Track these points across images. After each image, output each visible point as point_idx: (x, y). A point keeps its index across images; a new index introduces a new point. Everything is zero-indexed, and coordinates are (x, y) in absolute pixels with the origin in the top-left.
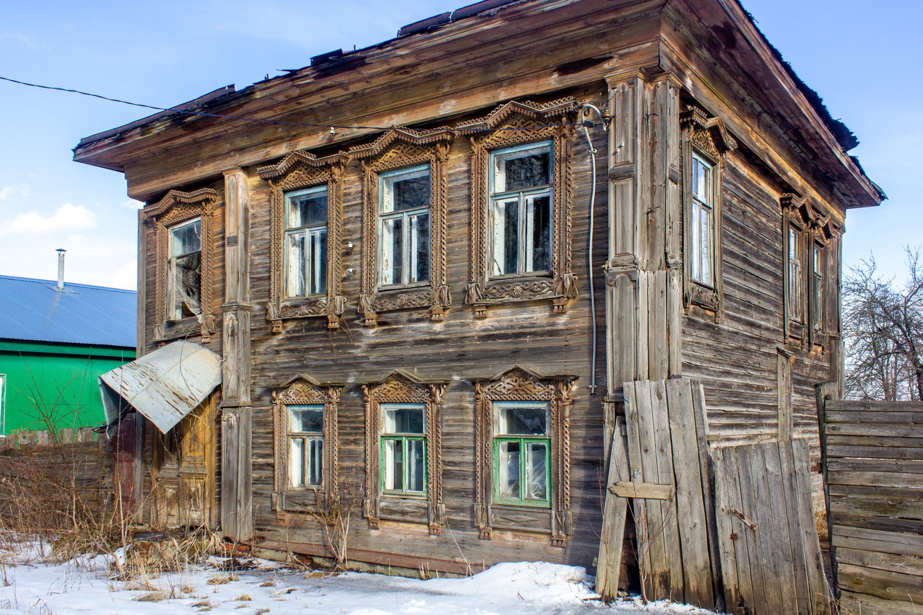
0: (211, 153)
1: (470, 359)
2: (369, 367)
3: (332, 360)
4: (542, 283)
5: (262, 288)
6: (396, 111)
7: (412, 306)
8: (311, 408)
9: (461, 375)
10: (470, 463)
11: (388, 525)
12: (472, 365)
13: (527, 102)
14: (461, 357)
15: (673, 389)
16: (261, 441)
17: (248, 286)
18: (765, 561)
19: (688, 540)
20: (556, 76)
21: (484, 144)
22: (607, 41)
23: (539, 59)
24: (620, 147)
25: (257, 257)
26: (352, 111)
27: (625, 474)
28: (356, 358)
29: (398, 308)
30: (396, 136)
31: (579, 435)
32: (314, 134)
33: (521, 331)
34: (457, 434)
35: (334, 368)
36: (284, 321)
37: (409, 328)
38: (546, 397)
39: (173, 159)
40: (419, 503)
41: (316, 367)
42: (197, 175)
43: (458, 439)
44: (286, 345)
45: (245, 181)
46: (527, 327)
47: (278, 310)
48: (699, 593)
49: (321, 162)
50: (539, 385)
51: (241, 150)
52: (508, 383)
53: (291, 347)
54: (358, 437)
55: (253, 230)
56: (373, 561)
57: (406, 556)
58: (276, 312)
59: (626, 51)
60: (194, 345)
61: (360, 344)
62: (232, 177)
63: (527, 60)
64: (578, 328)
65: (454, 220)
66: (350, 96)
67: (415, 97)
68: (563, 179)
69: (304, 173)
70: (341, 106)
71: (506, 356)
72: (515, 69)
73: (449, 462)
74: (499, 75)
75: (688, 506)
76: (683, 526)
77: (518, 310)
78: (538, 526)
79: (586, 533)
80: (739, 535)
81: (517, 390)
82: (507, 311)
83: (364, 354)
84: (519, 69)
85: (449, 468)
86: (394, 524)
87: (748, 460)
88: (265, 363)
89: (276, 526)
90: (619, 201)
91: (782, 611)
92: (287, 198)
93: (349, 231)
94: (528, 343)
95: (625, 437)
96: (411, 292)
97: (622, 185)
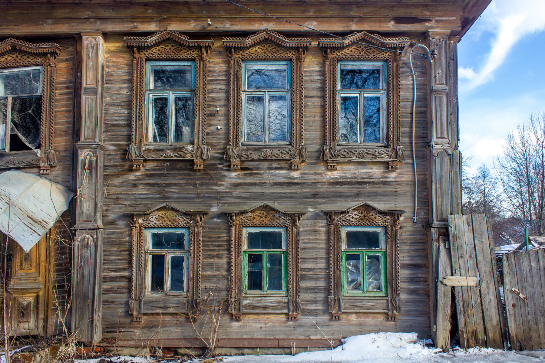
0: (68, 16)
1: (322, 198)
2: (233, 200)
3: (195, 194)
4: (381, 151)
6: (267, 19)
7: (275, 158)
8: (172, 231)
9: (315, 208)
10: (323, 269)
11: (249, 318)
12: (324, 202)
13: (375, 35)
14: (315, 195)
15: (476, 220)
16: (113, 257)
17: (103, 130)
18: (530, 318)
19: (487, 310)
20: (392, 23)
21: (240, 56)
22: (428, 10)
23: (382, 10)
24: (439, 74)
25: (112, 108)
26: (226, 11)
27: (449, 272)
28: (219, 193)
29: (262, 158)
30: (266, 37)
31: (406, 249)
32: (186, 21)
33: (362, 180)
34: (311, 249)
35: (197, 200)
36: (145, 161)
37: (269, 174)
38: (384, 224)
39: (17, 11)
40: (280, 299)
41: (178, 198)
42: (46, 31)
43: (311, 253)
44: (145, 180)
45: (103, 45)
46: (367, 178)
47: (140, 151)
48: (494, 340)
49: (193, 43)
50: (379, 216)
51: (103, 19)
52: (356, 215)
53: (151, 181)
54: (221, 253)
55: (108, 85)
56: (241, 345)
57: (266, 339)
58: (137, 153)
59: (440, 18)
60: (31, 175)
61: (223, 183)
62: (90, 39)
63: (374, 9)
64: (404, 181)
65: (308, 102)
67: (284, 13)
68: (395, 87)
69: (170, 49)
70: (215, 5)
71: (351, 196)
72: (364, 12)
73: (305, 269)
74: (353, 13)
75: (486, 289)
76: (485, 301)
77: (360, 167)
78: (378, 309)
79: (411, 311)
80: (516, 304)
81: (362, 219)
82: (352, 167)
83: (227, 191)
84: (368, 13)
85: (304, 273)
86: (255, 317)
87: (521, 261)
88: (121, 194)
89: (130, 328)
90: (438, 106)
91: (540, 345)
92: (148, 66)
93: (213, 98)
94: (368, 189)
95: (449, 250)
96: (274, 148)
97: (440, 97)
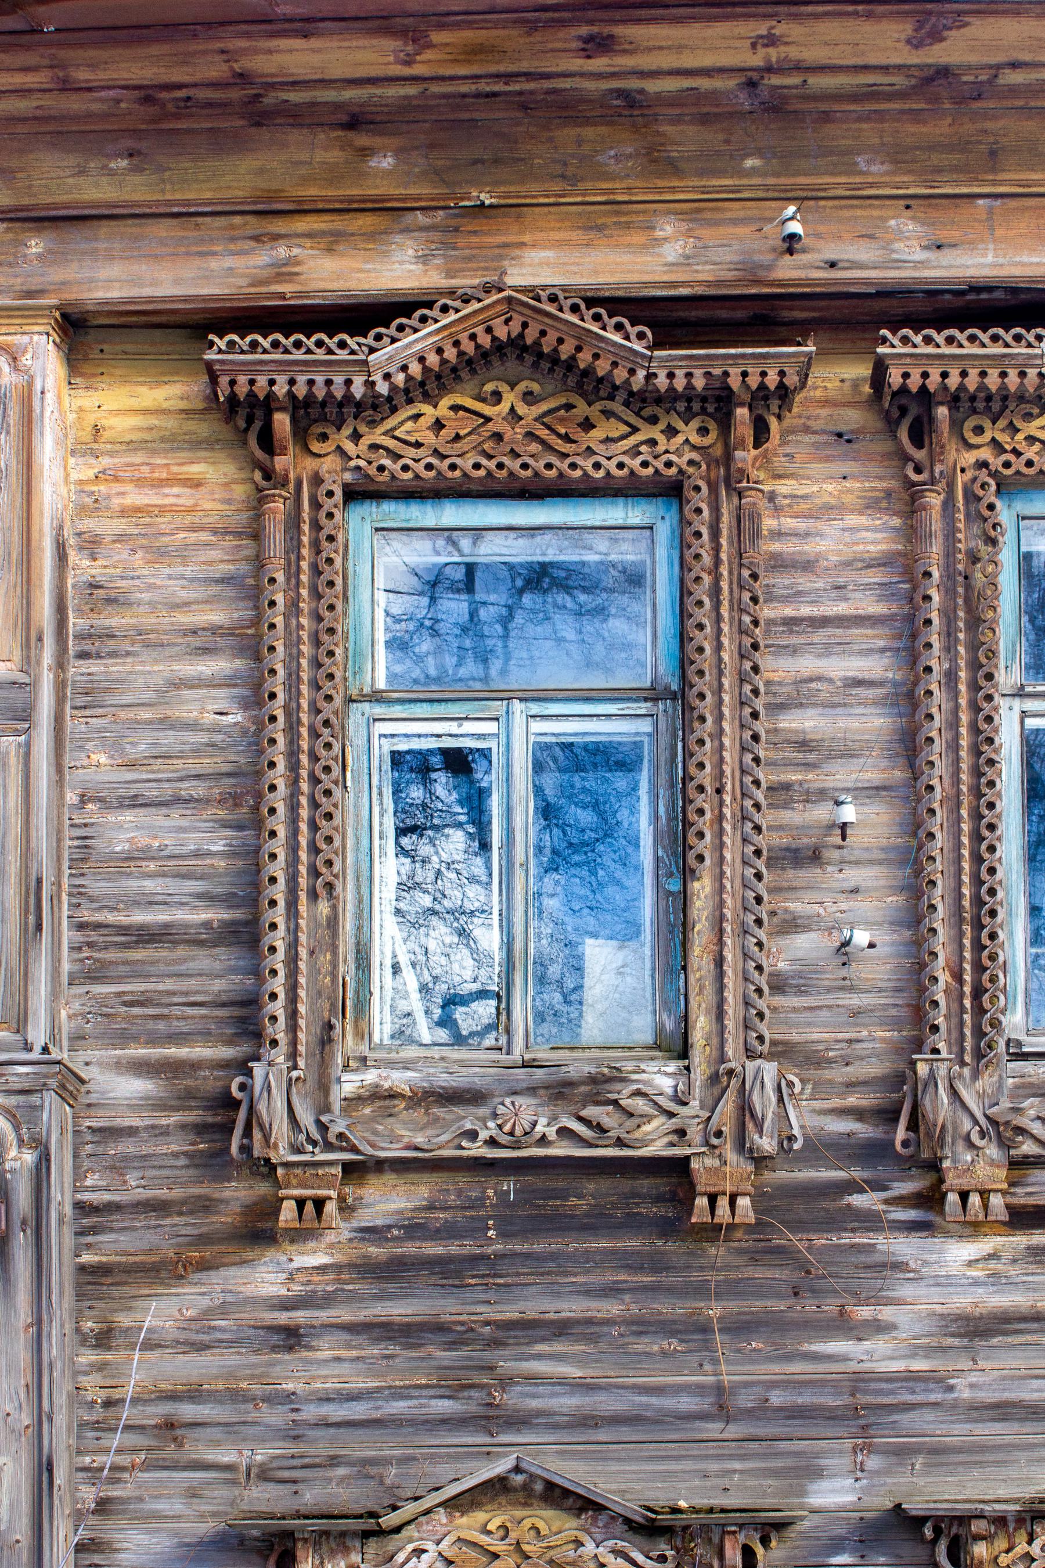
3: (699, 1390)
5: (169, 985)
21: (985, 454)
25: (128, 817)
28: (859, 1381)
44: (354, 1298)
53: (397, 1310)
55: (94, 667)
61: (887, 1313)
66: (899, 81)
70: (826, 117)
83: (919, 1365)
93: (804, 745)
